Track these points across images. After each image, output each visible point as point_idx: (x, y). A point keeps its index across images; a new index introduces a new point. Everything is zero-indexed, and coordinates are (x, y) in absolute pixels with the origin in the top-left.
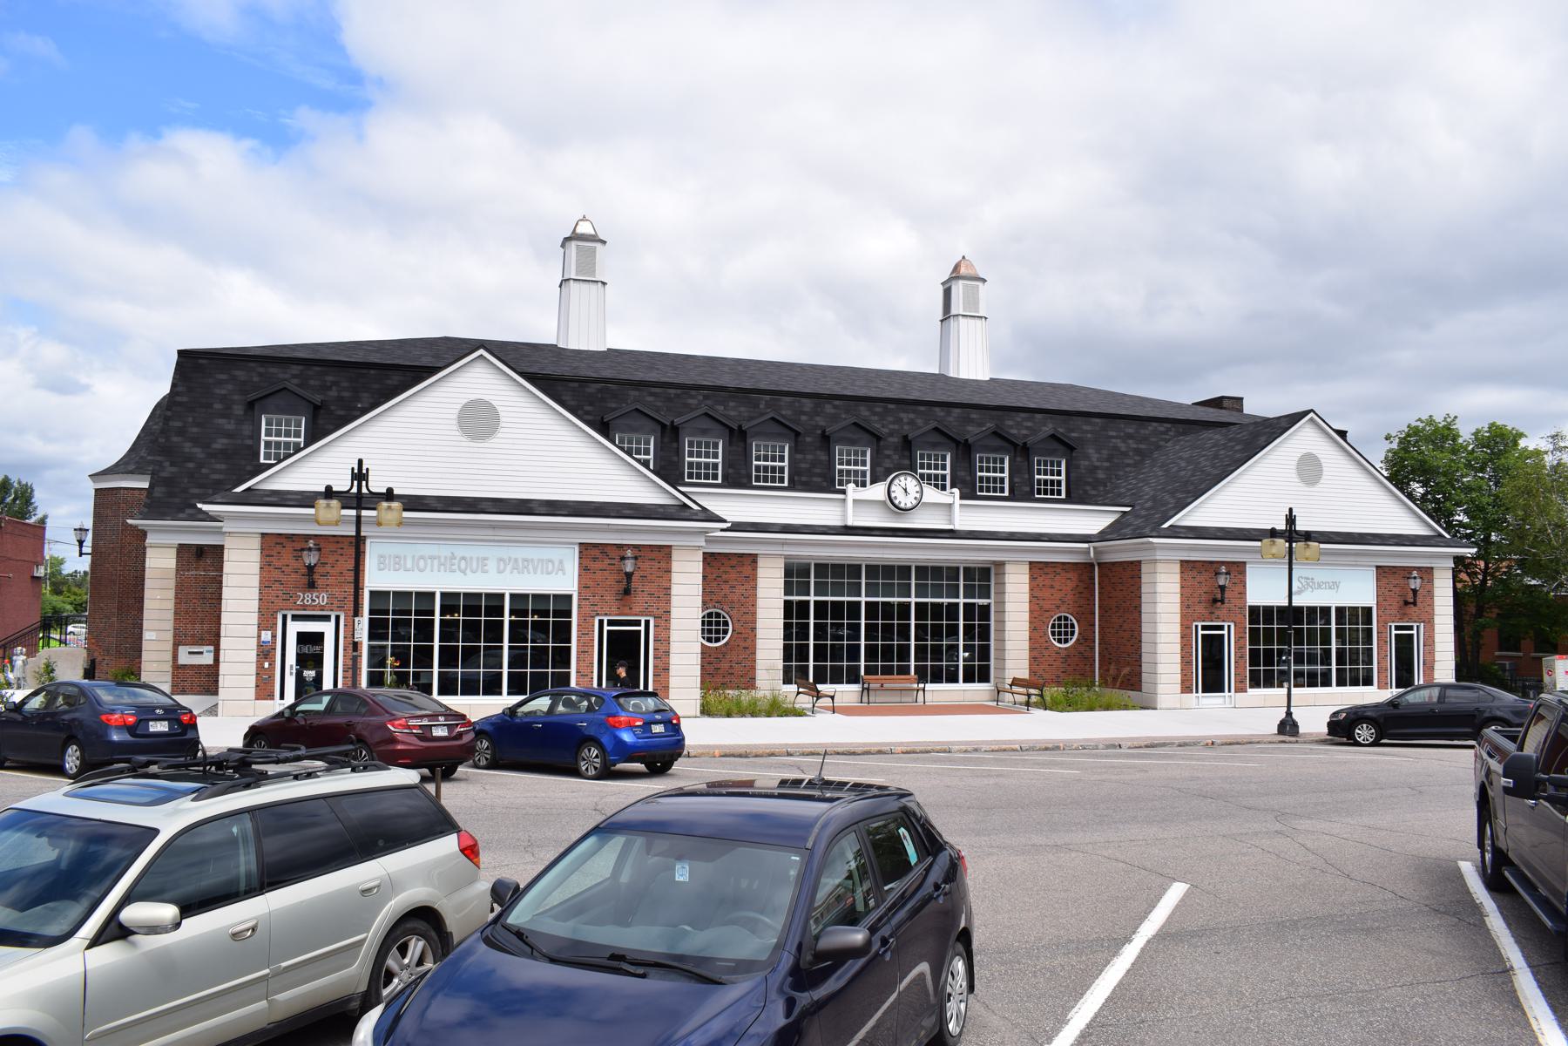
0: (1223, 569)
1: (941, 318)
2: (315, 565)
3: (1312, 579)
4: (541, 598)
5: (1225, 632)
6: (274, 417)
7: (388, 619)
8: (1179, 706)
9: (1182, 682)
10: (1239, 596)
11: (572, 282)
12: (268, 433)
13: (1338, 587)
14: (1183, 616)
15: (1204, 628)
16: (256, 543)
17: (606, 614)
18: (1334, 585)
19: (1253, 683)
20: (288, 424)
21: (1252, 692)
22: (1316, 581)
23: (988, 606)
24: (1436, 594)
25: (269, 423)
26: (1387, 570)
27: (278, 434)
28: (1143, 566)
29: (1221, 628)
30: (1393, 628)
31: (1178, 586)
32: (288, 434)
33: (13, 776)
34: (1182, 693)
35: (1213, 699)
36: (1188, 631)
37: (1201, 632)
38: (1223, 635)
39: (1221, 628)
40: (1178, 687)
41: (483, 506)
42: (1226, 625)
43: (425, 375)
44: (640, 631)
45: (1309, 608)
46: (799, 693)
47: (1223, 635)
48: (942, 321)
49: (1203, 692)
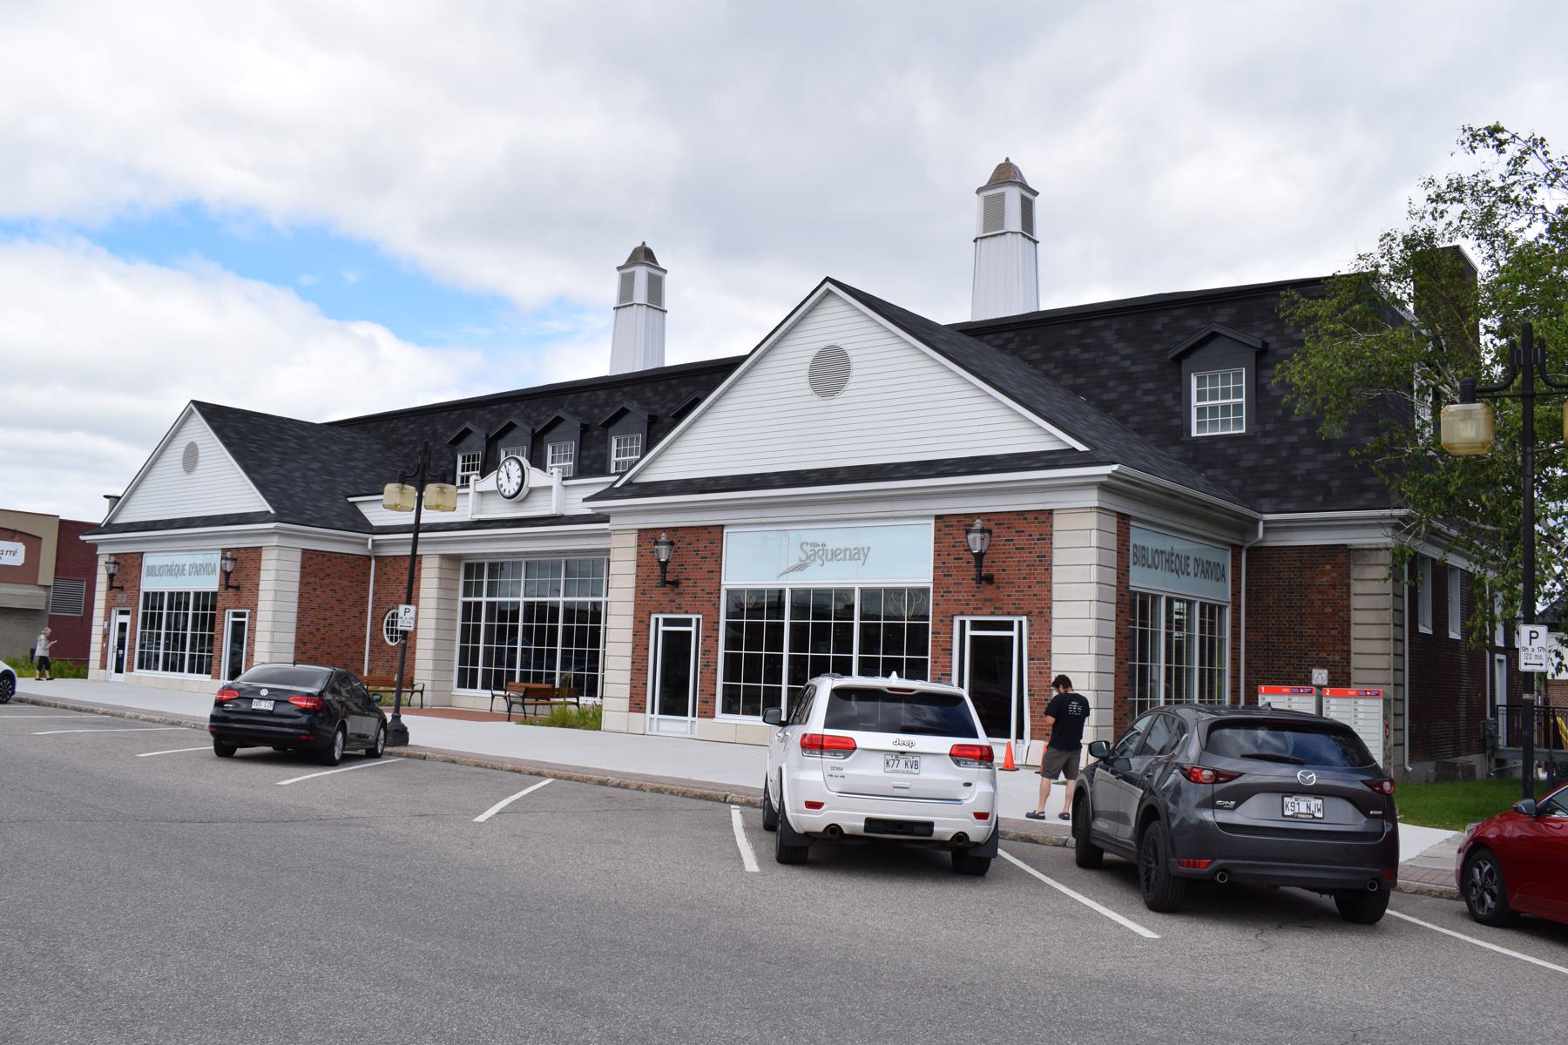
0: (663, 537)
1: (615, 304)
2: (231, 572)
3: (823, 545)
4: (822, 594)
5: (1015, 634)
6: (622, 438)
7: (831, 623)
8: (624, 729)
9: (631, 697)
10: (710, 575)
11: (635, 306)
12: (1201, 397)
13: (866, 556)
14: (637, 605)
15: (976, 625)
16: (298, 556)
17: (661, 612)
18: (859, 554)
19: (748, 707)
20: (1225, 381)
21: (722, 718)
22: (829, 547)
23: (465, 595)
24: (1055, 561)
25: (1201, 382)
26: (954, 522)
27: (1214, 396)
28: (264, 552)
29: (1009, 626)
30: (231, 615)
31: (633, 564)
32: (1226, 395)
33: (879, 812)
34: (630, 711)
35: (674, 725)
36: (643, 626)
37: (661, 628)
38: (1011, 638)
39: (1009, 626)
40: (626, 703)
41: (158, 526)
42: (1016, 620)
43: (718, 376)
44: (1012, 637)
45: (204, 593)
46: (493, 696)
47: (1011, 638)
48: (617, 308)
49: (660, 713)
